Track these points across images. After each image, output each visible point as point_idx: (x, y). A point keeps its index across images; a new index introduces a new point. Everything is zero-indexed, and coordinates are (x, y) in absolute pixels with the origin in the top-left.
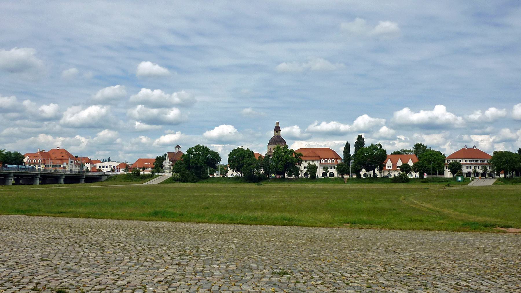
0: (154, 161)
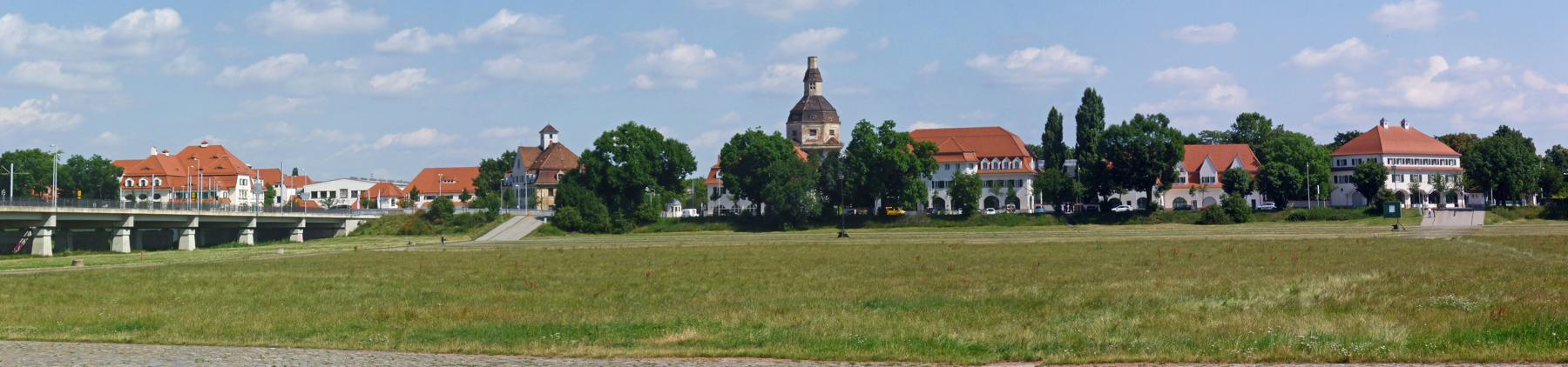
0: (476, 175)
